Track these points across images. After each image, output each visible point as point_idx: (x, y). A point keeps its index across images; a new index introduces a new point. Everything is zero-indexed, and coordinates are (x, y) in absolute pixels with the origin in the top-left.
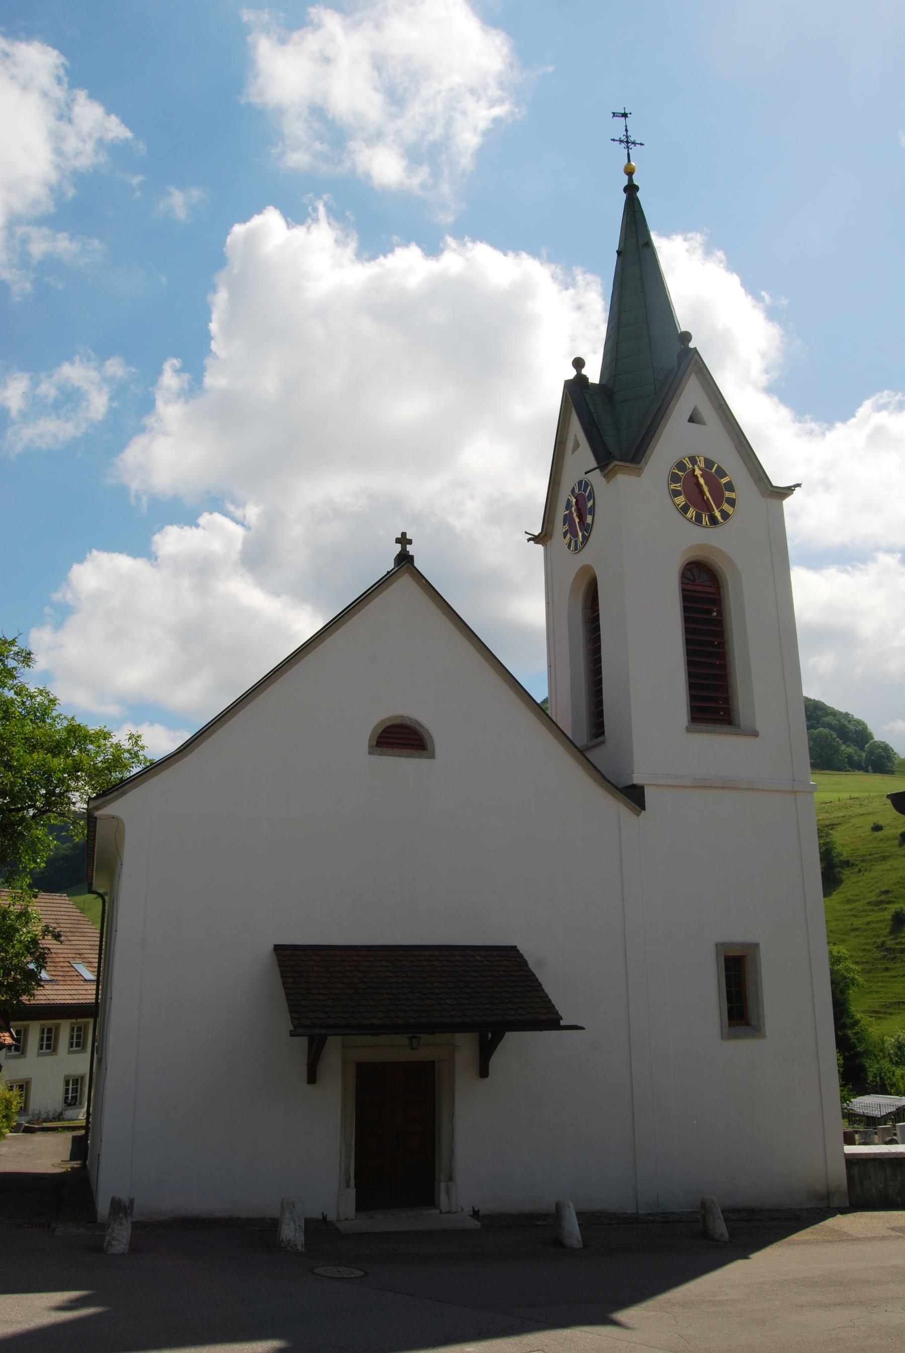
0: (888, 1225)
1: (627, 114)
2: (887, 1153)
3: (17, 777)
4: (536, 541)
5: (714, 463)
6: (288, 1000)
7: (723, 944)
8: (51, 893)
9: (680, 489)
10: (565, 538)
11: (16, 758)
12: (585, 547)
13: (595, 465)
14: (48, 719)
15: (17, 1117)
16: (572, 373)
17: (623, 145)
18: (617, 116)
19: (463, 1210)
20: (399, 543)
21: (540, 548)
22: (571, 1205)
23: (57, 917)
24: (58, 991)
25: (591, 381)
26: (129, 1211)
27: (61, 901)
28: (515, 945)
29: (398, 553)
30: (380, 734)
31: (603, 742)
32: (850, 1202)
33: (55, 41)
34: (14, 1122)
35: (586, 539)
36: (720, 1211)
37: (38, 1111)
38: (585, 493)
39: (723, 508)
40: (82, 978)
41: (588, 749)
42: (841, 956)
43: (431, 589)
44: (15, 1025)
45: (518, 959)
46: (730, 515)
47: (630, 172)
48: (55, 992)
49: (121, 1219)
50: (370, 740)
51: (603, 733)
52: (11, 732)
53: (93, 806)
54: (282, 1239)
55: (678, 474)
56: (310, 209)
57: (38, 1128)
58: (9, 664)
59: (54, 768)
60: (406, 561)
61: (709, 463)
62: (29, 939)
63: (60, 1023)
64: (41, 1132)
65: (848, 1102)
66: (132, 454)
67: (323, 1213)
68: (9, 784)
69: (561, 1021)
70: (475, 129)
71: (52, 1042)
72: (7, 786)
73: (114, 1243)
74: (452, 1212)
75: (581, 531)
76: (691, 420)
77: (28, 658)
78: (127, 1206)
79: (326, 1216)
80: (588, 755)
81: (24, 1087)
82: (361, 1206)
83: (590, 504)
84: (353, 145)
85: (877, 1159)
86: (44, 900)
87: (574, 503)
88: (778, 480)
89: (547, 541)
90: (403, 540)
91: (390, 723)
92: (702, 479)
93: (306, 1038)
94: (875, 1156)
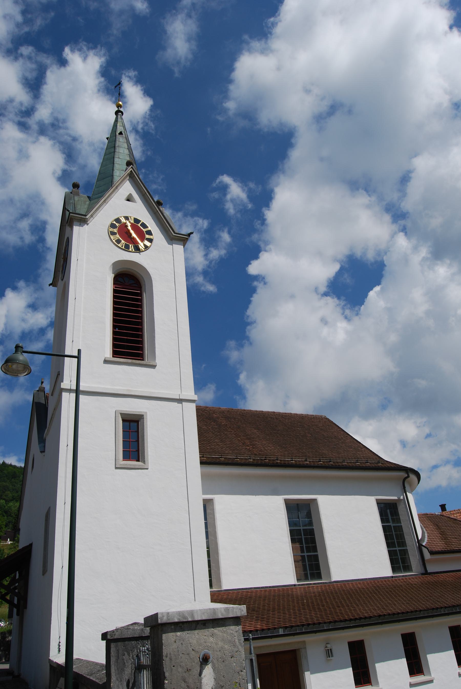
46: (153, 239)
53: (9, 598)
61: (137, 221)
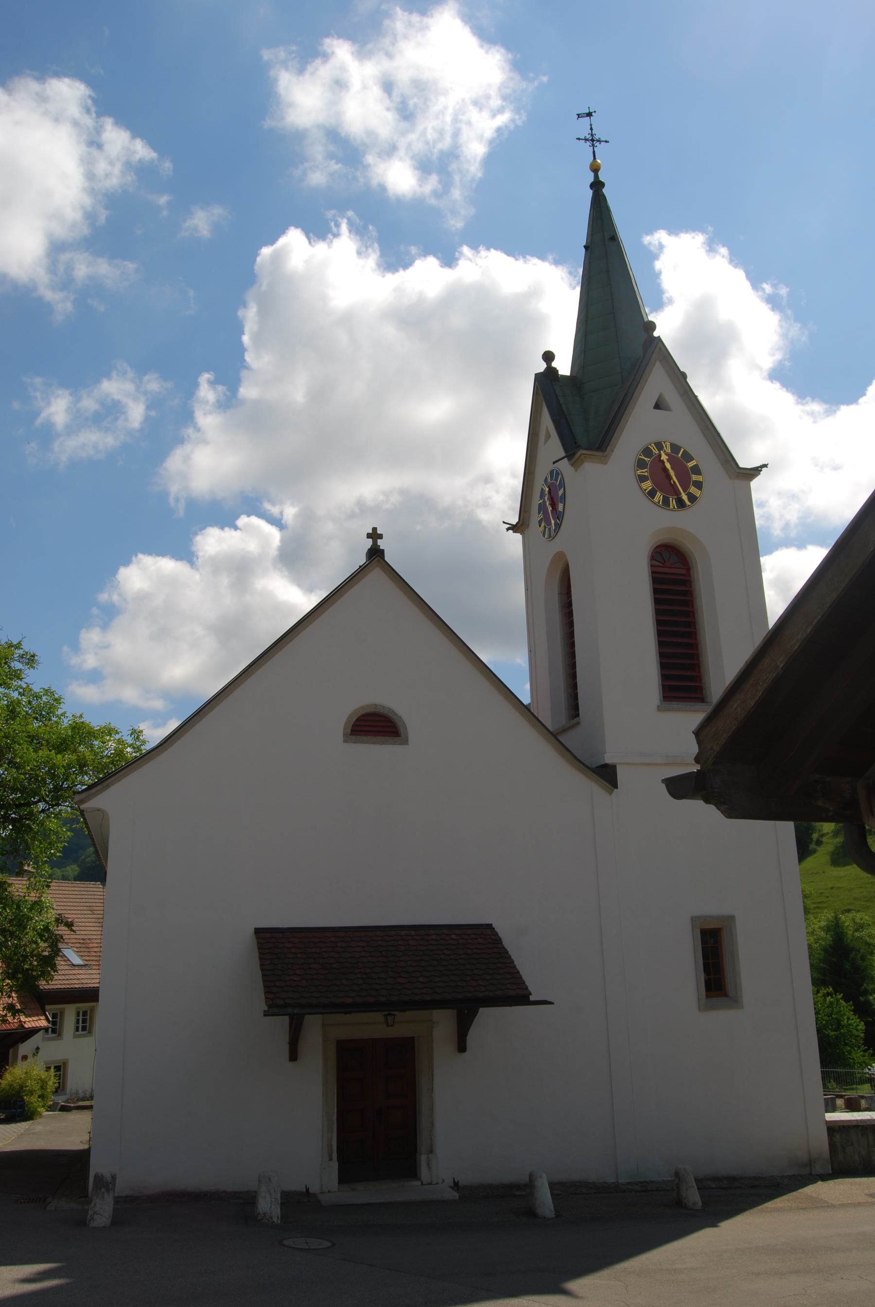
0: (866, 1192)
1: (592, 113)
2: (869, 1120)
3: (21, 774)
4: (514, 530)
5: (679, 448)
6: (264, 981)
7: (698, 918)
8: (85, 881)
9: (646, 474)
10: (540, 526)
11: (20, 755)
12: (558, 534)
13: (563, 454)
14: (54, 717)
15: (53, 1097)
16: (542, 367)
17: (589, 143)
18: (581, 117)
19: (443, 1181)
20: (370, 538)
21: (518, 536)
22: (544, 1175)
23: (91, 904)
24: (91, 975)
25: (560, 373)
26: (111, 1186)
27: (95, 889)
28: (491, 923)
29: (369, 547)
30: (354, 722)
31: (578, 724)
32: (833, 1169)
33: (79, 75)
34: (50, 1101)
35: (558, 526)
36: (693, 1179)
37: (76, 1091)
38: (557, 481)
39: (690, 491)
40: (70, 963)
41: (565, 730)
42: (864, 923)
43: (401, 581)
44: (50, 1009)
45: (492, 937)
47: (595, 169)
48: (88, 976)
49: (103, 1193)
50: (344, 729)
51: (578, 715)
52: (14, 731)
54: (259, 1211)
55: (644, 459)
56: (332, 224)
57: (74, 1107)
58: (15, 666)
59: (58, 763)
60: (376, 555)
61: (675, 448)
62: (42, 927)
63: (64, 1009)
64: (76, 1111)
65: (869, 1067)
66: (174, 462)
67: (306, 1186)
68: (12, 780)
69: (531, 997)
70: (480, 138)
71: (88, 1024)
72: (10, 783)
73: (96, 1216)
74: (433, 1183)
75: (554, 520)
76: (657, 406)
77: (32, 660)
78: (109, 1181)
79: (308, 1188)
80: (562, 738)
81: (60, 1069)
82: (344, 1178)
83: (561, 492)
84: (370, 159)
85: (859, 1126)
86: (79, 888)
87: (547, 492)
88: (745, 461)
89: (525, 530)
90: (374, 535)
91: (364, 712)
92: (668, 464)
93: (287, 1018)
94: (857, 1123)
